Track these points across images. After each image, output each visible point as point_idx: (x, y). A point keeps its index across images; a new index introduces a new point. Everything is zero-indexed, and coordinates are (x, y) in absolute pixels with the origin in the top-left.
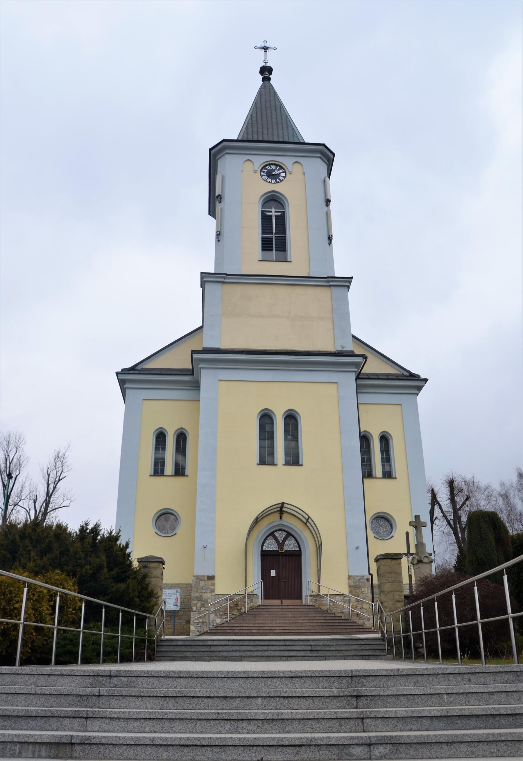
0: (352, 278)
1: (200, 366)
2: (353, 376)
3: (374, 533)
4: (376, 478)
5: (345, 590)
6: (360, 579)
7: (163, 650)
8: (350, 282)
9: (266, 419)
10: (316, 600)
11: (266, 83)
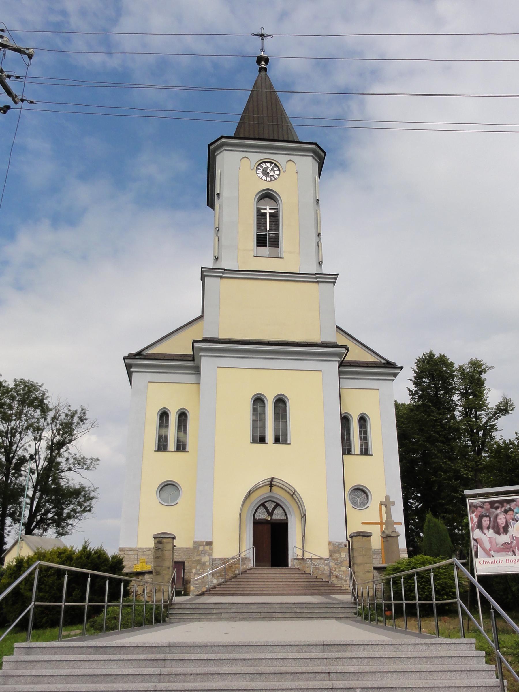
0: (338, 274)
1: (200, 354)
2: (336, 365)
3: (352, 503)
4: (354, 455)
5: (325, 554)
6: (338, 545)
7: (175, 612)
8: (336, 279)
9: (259, 401)
10: (301, 563)
11: (263, 73)
